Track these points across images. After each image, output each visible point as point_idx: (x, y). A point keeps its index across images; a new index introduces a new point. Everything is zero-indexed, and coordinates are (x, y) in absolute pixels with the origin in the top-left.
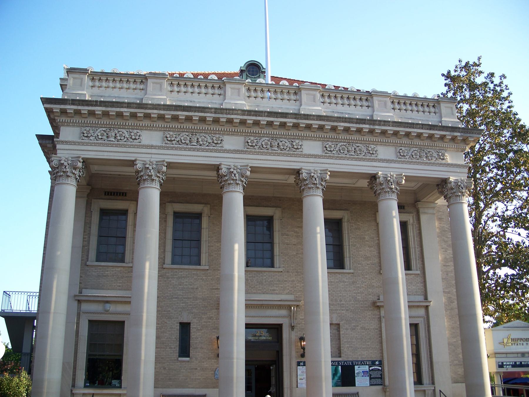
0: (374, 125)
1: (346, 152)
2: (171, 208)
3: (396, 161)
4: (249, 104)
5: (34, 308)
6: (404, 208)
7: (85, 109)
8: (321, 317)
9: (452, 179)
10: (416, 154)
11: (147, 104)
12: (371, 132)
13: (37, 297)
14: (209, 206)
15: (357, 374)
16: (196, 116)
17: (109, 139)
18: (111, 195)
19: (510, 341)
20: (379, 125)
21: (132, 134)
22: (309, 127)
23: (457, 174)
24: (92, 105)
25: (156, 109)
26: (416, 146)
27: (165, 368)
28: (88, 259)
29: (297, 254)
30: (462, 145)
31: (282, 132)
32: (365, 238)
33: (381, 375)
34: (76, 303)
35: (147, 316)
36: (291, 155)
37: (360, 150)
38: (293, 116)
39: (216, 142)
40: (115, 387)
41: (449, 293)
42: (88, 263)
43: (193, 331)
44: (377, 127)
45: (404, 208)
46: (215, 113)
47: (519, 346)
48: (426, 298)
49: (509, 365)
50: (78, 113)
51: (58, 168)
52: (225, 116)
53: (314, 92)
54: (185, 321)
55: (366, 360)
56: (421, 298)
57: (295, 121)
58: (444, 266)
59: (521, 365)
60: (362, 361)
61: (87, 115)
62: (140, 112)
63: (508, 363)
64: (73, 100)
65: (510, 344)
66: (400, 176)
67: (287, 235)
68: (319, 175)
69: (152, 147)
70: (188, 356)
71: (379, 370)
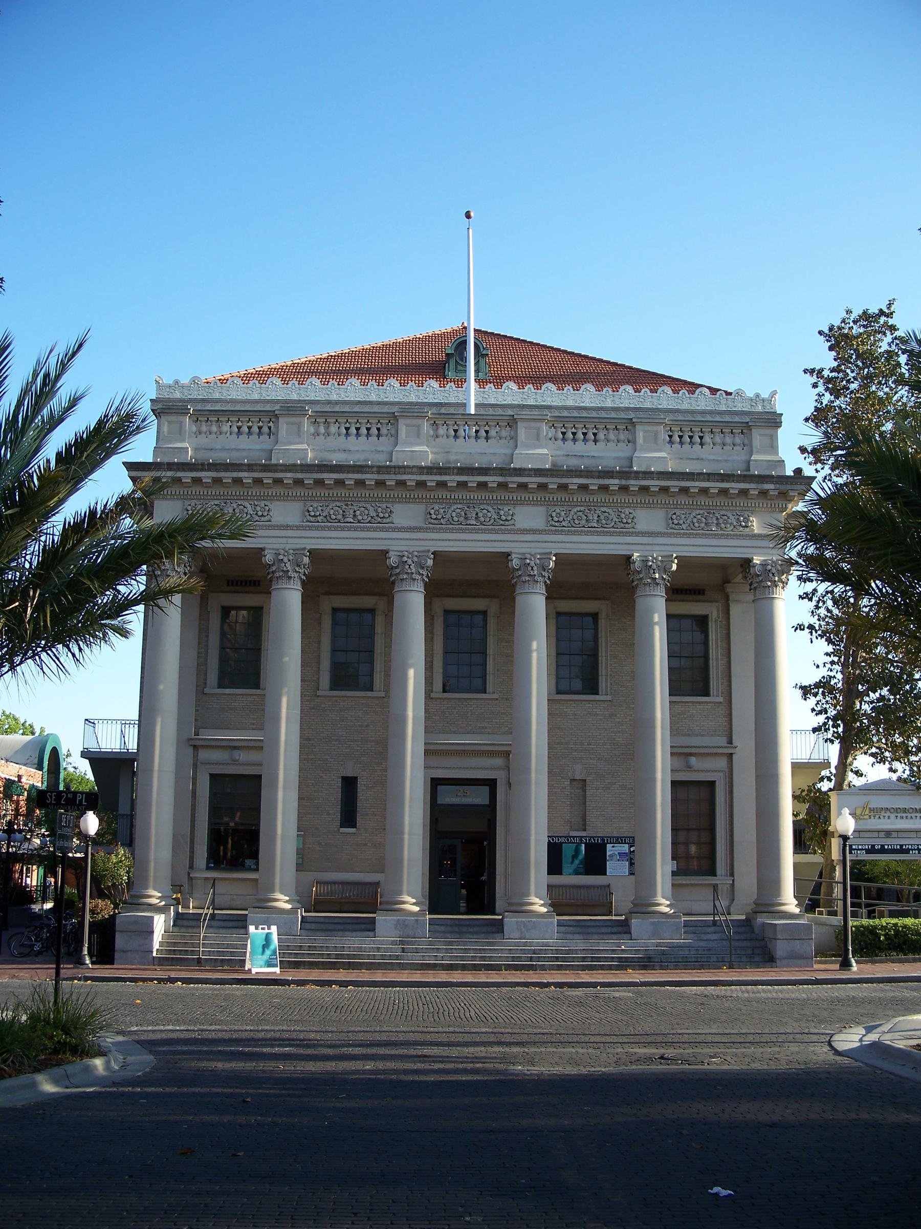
0: (627, 479)
1: (583, 522)
2: (328, 603)
3: (665, 533)
4: (435, 450)
5: (133, 746)
6: (704, 594)
7: (187, 476)
8: (533, 775)
9: (757, 560)
10: (699, 521)
11: (276, 465)
12: (624, 489)
13: (136, 726)
15: (610, 856)
16: (350, 478)
17: (468, 522)
18: (237, 585)
19: (867, 812)
20: (637, 478)
21: (258, 508)
22: (523, 486)
23: (765, 551)
24: (197, 470)
25: (290, 471)
26: (701, 507)
27: (320, 844)
28: (205, 684)
30: (781, 503)
31: (483, 495)
34: (191, 750)
35: (285, 774)
36: (496, 532)
37: (607, 519)
39: (381, 515)
40: (250, 870)
42: (206, 690)
43: (361, 788)
44: (632, 482)
45: (704, 594)
46: (378, 473)
47: (882, 820)
48: (730, 742)
50: (543, 487)
52: (393, 477)
53: (538, 424)
56: (722, 741)
59: (882, 850)
60: (618, 838)
61: (353, 487)
62: (267, 477)
64: (168, 464)
65: (867, 817)
66: (668, 559)
68: (538, 562)
69: (287, 527)
70: (354, 826)
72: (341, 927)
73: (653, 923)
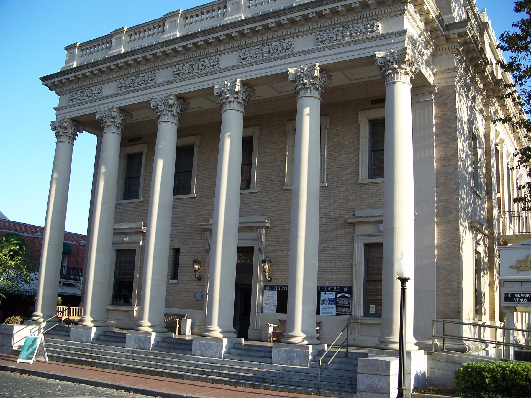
0: (279, 16)
14: (199, 136)
15: (322, 301)
20: (285, 14)
29: (272, 172)
32: (344, 144)
33: (349, 303)
38: (202, 34)
41: (446, 201)
43: (181, 255)
49: (524, 298)
51: (384, 66)
54: (176, 247)
55: (334, 285)
57: (204, 38)
58: (443, 166)
60: (328, 287)
63: (522, 296)
67: (264, 154)
70: (177, 279)
71: (347, 297)
72: (115, 339)
73: (287, 351)
